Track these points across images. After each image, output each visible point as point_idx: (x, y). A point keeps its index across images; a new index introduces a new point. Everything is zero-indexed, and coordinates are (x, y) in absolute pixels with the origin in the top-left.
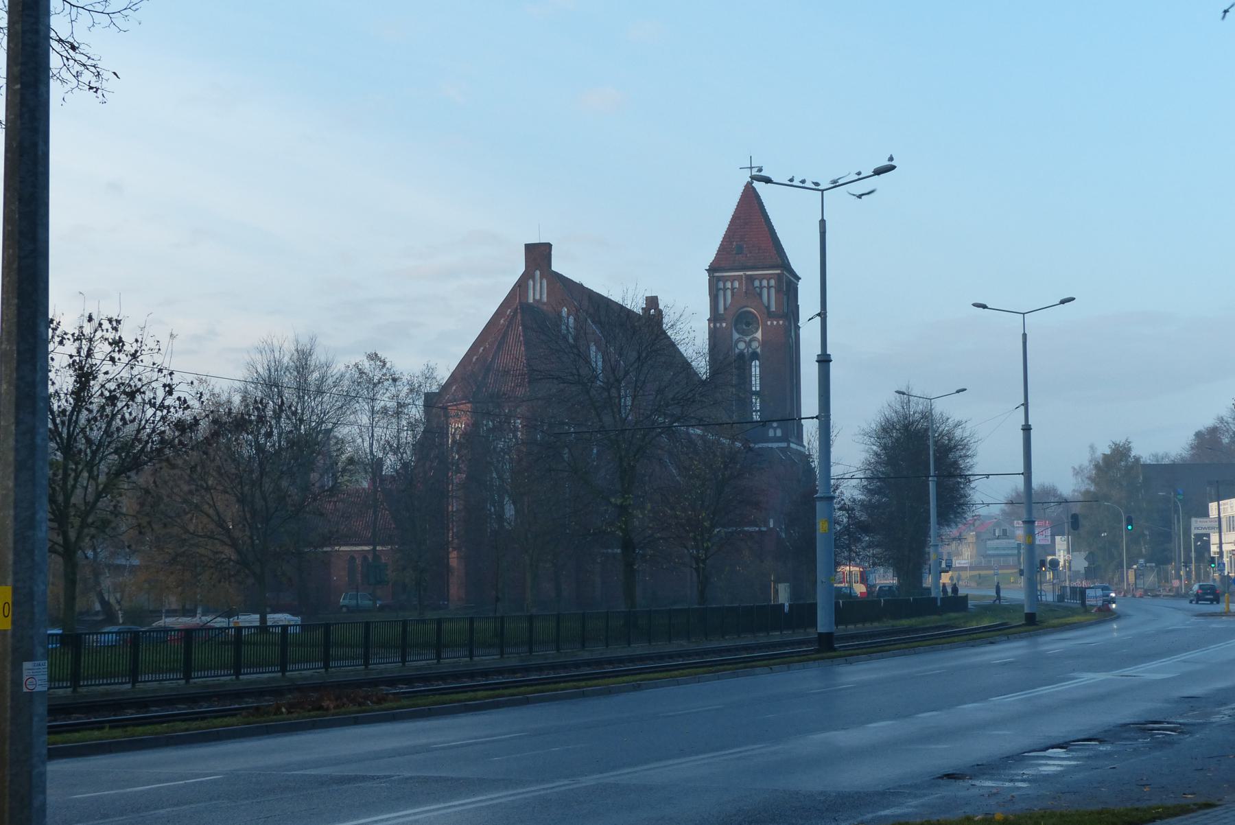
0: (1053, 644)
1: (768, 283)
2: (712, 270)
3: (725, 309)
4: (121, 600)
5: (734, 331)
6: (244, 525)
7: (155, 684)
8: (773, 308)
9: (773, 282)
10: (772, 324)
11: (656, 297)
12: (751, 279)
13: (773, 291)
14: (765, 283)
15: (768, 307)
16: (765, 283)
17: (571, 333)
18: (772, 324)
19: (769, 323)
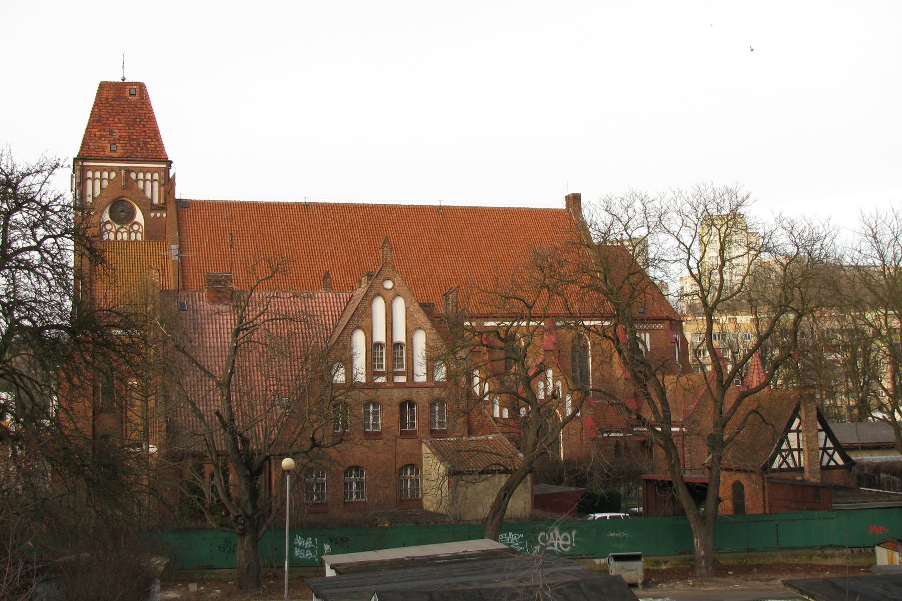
0: (753, 554)
1: (152, 177)
2: (75, 159)
3: (94, 199)
4: (506, 471)
5: (107, 210)
6: (104, 354)
7: (654, 592)
8: (156, 201)
9: (156, 176)
10: (155, 215)
11: (103, 86)
12: (128, 171)
13: (156, 184)
14: (149, 176)
15: (151, 200)
16: (141, 176)
17: (52, 377)
18: (155, 215)
19: (152, 215)
